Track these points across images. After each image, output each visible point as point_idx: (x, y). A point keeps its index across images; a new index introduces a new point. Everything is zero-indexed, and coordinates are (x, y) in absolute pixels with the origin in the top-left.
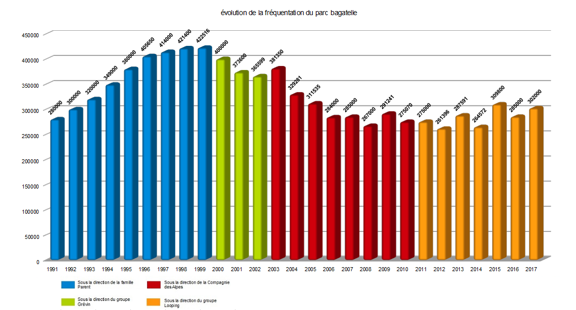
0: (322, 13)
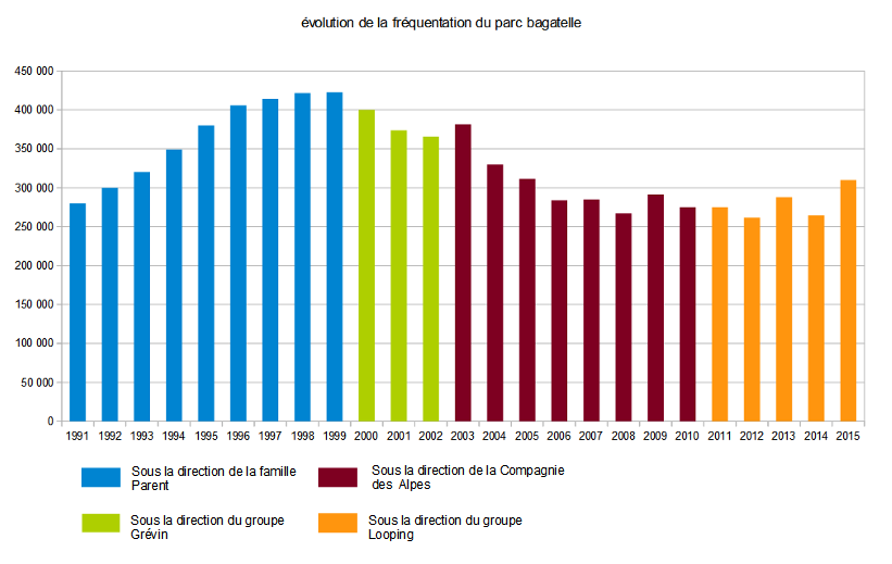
0: (510, 23)
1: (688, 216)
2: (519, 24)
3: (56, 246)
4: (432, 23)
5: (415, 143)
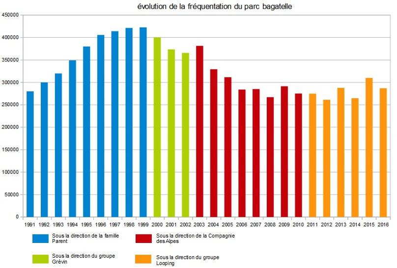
1: (299, 97)
2: (258, 7)
3: (19, 116)
4: (210, 6)
5: (178, 56)
